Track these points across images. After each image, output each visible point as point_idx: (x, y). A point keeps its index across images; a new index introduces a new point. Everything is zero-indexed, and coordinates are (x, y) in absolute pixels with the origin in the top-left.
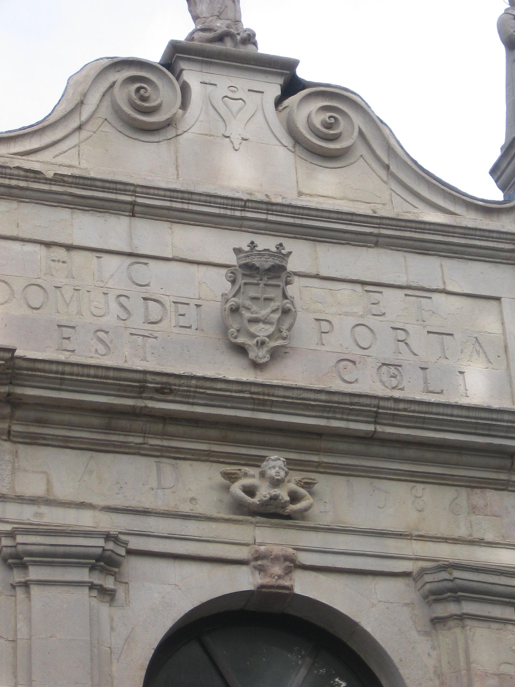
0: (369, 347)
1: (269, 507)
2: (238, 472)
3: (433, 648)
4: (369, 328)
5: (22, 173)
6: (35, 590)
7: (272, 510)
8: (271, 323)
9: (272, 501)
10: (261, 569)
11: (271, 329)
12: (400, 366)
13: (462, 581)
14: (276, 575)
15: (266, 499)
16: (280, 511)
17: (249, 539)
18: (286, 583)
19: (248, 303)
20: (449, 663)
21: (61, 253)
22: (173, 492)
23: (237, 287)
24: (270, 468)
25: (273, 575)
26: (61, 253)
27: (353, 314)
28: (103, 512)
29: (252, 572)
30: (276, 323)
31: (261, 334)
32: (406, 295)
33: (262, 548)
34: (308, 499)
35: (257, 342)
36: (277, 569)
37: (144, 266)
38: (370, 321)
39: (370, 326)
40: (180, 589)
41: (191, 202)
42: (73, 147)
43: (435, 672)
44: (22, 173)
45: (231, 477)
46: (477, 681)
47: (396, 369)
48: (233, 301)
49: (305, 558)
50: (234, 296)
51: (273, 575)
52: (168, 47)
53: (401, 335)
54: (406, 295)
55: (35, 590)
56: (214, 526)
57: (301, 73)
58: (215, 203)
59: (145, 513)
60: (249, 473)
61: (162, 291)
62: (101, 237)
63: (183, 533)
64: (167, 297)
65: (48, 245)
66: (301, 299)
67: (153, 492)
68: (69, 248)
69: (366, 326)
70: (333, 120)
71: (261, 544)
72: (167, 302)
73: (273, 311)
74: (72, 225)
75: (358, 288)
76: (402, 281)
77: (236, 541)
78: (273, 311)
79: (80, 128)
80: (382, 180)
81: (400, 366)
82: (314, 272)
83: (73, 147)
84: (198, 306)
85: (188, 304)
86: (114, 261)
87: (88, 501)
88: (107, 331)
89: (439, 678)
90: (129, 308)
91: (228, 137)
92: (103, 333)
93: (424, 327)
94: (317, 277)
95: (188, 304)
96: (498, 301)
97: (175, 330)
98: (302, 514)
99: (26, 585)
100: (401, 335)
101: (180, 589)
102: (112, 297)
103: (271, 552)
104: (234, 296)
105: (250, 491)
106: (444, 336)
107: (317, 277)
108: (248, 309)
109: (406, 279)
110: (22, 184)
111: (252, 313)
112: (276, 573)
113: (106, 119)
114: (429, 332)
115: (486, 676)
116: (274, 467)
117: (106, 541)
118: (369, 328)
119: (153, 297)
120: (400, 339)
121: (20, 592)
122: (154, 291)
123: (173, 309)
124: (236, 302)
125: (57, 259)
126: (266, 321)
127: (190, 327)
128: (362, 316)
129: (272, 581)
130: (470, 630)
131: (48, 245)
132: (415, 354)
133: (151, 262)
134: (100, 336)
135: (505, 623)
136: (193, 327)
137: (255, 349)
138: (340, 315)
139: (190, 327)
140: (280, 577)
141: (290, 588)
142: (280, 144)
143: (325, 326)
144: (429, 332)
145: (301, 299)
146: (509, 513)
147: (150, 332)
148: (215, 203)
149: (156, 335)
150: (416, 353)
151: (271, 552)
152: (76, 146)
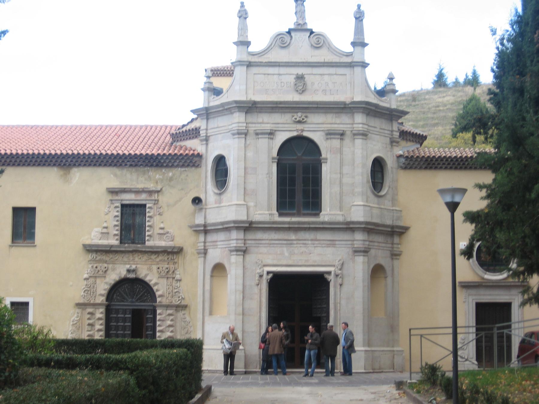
10: (298, 132)
18: (302, 134)
26: (267, 76)
45: (293, 116)
49: (305, 129)
57: (314, 30)
59: (278, 124)
65: (265, 74)
68: (268, 74)
79: (272, 48)
86: (275, 76)
94: (312, 74)
98: (305, 122)
99: (259, 138)
105: (296, 119)
107: (312, 74)
126: (301, 86)
131: (265, 74)
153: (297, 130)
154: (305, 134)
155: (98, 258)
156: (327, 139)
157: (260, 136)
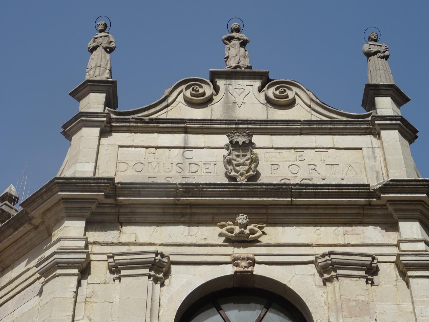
0: (288, 168)
1: (240, 237)
2: (225, 224)
3: (324, 293)
4: (298, 166)
5: (134, 120)
6: (122, 279)
7: (242, 239)
8: (247, 165)
9: (241, 235)
10: (237, 265)
11: (247, 167)
12: (312, 179)
13: (335, 259)
14: (243, 266)
15: (237, 233)
16: (246, 239)
17: (231, 252)
19: (235, 157)
20: (331, 298)
21: (153, 150)
22: (196, 237)
23: (229, 151)
24: (239, 220)
25: (242, 266)
27: (289, 161)
28: (160, 246)
29: (233, 267)
30: (248, 165)
31: (242, 170)
32: (315, 151)
33: (236, 255)
34: (259, 232)
35: (240, 173)
36: (244, 264)
37: (191, 151)
38: (298, 163)
39: (298, 165)
40: (196, 276)
41: (212, 124)
42: (164, 113)
43: (325, 303)
44: (134, 120)
46: (344, 304)
47: (310, 180)
48: (228, 158)
49: (258, 259)
50: (228, 155)
51: (242, 266)
52: (210, 73)
53: (313, 167)
54: (315, 151)
55: (122, 279)
56: (214, 248)
57: (270, 77)
58: (223, 123)
60: (230, 224)
61: (199, 160)
62: (171, 142)
63: (199, 252)
64: (201, 162)
65: (147, 148)
66: (264, 157)
67: (186, 237)
68: (157, 148)
69: (296, 165)
70: (283, 90)
71: (236, 254)
72: (200, 164)
73: (247, 160)
74: (158, 139)
75: (292, 150)
76: (314, 146)
77: (224, 254)
78: (247, 160)
80: (308, 112)
81: (312, 179)
82: (271, 146)
83: (164, 113)
84: (215, 164)
85: (211, 164)
87: (152, 242)
88: (171, 177)
89: (327, 306)
90: (182, 168)
91: (236, 103)
92: (169, 178)
93: (324, 163)
95: (211, 164)
96: (361, 150)
97: (203, 174)
99: (119, 279)
100: (313, 167)
101: (196, 276)
102: (174, 164)
103: (241, 256)
104: (228, 155)
105: (231, 231)
106: (334, 166)
108: (235, 160)
109: (315, 145)
110: (134, 124)
111: (237, 162)
112: (243, 265)
113: (180, 102)
114: (326, 165)
115: (349, 301)
116: (241, 219)
117: (117, 229)
118: (298, 166)
119: (194, 163)
120: (312, 168)
121: (117, 281)
122: (194, 160)
123: (203, 166)
124: (229, 158)
125: (150, 152)
126: (243, 164)
127: (211, 173)
128: (294, 161)
129: (241, 269)
130: (341, 281)
131: (147, 148)
132: (319, 174)
133: (194, 150)
134: (168, 180)
135: (360, 278)
136: (212, 172)
137: (240, 177)
138: (283, 162)
139: (211, 173)
140: (245, 267)
141: (252, 272)
142: (260, 103)
143: (276, 167)
144: (326, 165)
145: (264, 157)
146: (364, 232)
147: (192, 176)
148: (223, 123)
149: (194, 177)
150: (320, 173)
151: (241, 256)
152: (165, 112)
153: (235, 261)
154: (258, 270)
155: (31, 199)
156: (325, 281)
157: (123, 272)
